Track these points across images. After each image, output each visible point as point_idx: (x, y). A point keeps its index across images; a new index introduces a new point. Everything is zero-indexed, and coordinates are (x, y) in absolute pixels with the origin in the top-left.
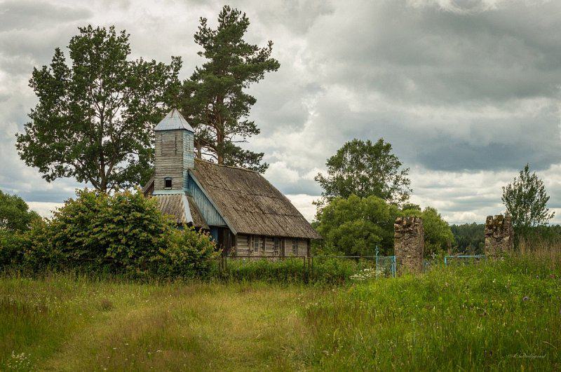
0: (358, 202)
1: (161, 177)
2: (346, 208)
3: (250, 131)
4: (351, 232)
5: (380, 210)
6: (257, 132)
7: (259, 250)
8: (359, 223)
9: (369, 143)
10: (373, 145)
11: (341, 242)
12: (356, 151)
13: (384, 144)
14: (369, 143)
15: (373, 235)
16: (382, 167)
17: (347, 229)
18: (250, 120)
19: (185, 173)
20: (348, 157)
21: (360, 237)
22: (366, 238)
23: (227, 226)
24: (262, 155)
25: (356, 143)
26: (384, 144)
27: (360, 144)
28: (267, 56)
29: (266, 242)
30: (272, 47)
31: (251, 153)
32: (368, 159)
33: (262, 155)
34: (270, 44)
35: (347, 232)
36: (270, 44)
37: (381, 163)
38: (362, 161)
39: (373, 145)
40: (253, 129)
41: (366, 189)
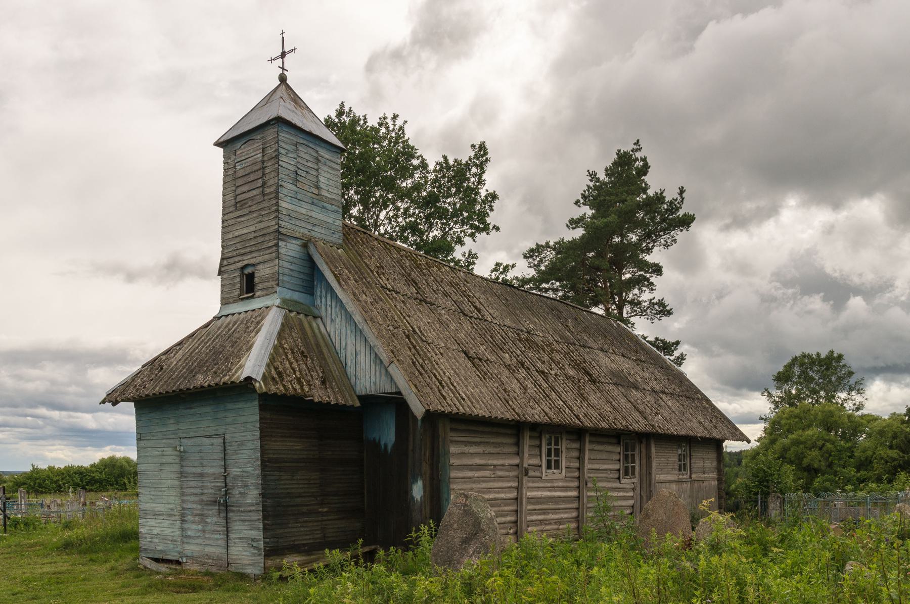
0: (809, 410)
1: (233, 267)
2: (796, 417)
3: (660, 312)
4: (802, 443)
5: (836, 418)
6: (669, 313)
7: (564, 464)
8: (815, 431)
9: (818, 354)
10: (823, 356)
11: (790, 454)
12: (805, 364)
13: (835, 355)
14: (818, 354)
15: (829, 445)
16: (834, 379)
17: (797, 440)
18: (657, 296)
19: (291, 249)
20: (797, 370)
21: (813, 447)
22: (821, 449)
23: (399, 393)
24: (677, 343)
25: (804, 356)
26: (835, 355)
27: (809, 356)
28: (677, 209)
29: (588, 446)
30: (684, 195)
31: (663, 341)
32: (818, 371)
33: (677, 343)
34: (682, 191)
35: (796, 443)
36: (682, 191)
37: (833, 374)
38: (811, 374)
39: (823, 356)
40: (662, 310)
41: (817, 401)
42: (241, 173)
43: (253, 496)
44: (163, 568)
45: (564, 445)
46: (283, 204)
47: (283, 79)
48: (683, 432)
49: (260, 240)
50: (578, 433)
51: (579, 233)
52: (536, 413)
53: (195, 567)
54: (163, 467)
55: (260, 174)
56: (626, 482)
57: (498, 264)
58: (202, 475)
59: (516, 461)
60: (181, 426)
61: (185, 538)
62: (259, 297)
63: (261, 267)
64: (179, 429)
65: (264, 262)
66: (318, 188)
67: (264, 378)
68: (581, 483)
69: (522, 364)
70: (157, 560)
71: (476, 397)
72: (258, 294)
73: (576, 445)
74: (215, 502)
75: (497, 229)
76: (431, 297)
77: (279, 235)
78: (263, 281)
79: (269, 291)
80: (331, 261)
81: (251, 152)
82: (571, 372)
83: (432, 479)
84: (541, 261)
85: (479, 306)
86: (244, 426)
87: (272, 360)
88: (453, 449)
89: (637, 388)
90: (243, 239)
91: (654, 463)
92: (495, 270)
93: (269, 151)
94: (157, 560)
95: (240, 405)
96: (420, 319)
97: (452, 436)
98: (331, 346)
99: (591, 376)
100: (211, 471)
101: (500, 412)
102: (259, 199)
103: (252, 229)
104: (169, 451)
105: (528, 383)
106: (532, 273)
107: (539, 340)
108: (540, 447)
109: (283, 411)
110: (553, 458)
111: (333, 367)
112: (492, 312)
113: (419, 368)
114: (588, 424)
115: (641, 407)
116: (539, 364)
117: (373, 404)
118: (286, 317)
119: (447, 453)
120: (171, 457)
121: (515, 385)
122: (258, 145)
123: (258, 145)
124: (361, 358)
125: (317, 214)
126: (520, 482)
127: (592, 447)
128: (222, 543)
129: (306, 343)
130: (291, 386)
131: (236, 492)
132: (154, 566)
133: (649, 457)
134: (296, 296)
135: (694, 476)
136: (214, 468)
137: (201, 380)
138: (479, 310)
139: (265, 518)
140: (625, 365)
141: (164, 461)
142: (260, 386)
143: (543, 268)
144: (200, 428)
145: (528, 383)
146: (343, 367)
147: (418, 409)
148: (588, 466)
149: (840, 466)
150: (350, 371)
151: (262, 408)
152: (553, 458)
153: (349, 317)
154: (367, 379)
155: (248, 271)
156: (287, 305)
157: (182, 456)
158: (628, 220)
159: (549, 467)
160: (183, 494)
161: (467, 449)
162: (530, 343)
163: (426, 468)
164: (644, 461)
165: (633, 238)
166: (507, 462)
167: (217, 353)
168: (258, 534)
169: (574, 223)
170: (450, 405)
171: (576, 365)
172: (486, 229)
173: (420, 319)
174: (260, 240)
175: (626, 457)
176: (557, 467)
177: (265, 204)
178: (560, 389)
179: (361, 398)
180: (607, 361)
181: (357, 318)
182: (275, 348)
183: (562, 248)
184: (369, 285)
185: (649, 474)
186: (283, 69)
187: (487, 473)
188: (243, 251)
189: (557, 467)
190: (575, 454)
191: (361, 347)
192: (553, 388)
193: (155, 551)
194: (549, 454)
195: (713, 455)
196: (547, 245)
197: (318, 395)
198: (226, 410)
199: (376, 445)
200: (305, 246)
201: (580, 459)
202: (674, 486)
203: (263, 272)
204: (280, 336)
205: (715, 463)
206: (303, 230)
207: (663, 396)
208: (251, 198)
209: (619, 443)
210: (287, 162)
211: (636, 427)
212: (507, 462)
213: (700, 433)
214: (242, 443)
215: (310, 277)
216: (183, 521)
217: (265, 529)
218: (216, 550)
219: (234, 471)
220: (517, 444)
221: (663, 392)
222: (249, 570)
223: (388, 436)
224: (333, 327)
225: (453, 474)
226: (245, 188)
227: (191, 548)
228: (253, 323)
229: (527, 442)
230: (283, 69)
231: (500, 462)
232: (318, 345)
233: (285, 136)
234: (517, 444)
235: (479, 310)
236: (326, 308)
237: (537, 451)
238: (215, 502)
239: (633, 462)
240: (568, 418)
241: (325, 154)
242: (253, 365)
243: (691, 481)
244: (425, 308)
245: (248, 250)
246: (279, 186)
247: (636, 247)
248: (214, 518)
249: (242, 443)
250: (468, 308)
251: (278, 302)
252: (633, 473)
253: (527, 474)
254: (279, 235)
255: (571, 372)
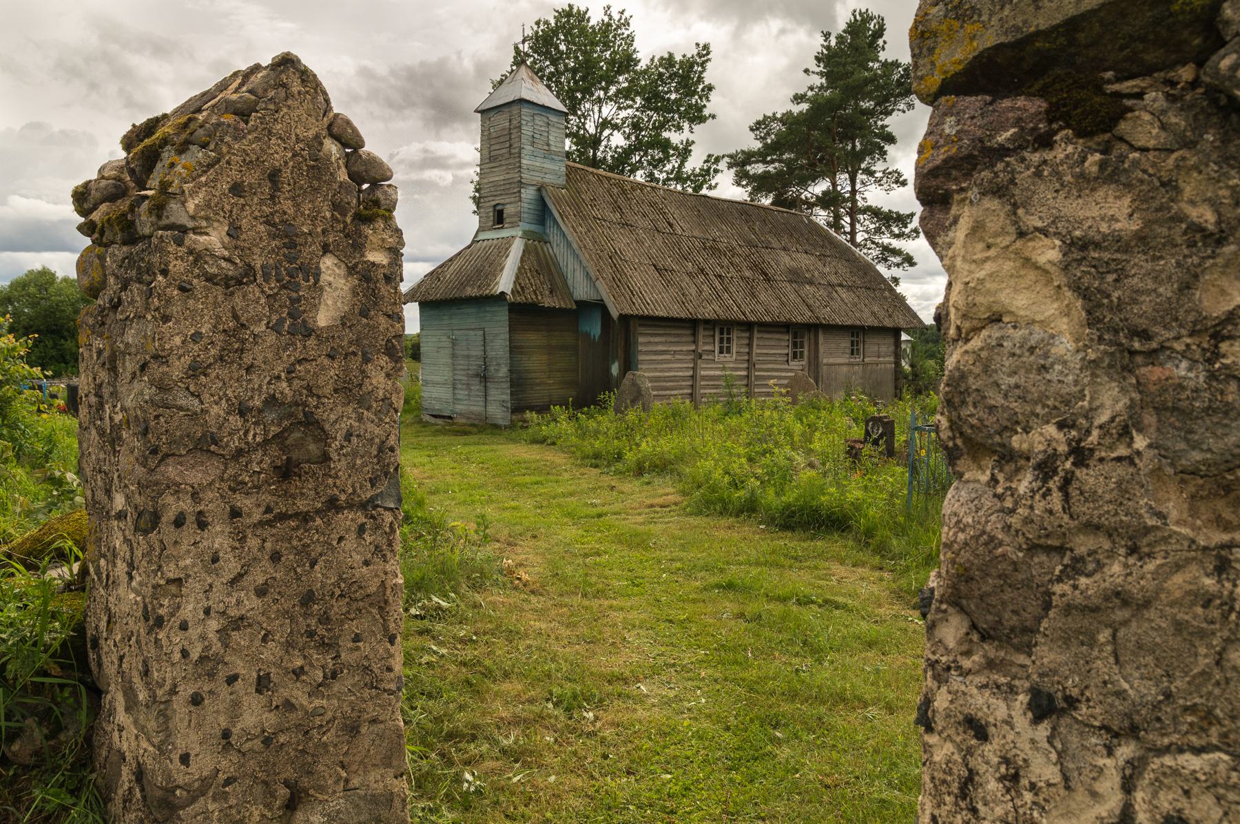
7: (734, 350)
19: (528, 194)
29: (756, 335)
42: (494, 135)
43: (504, 371)
44: (440, 421)
45: (735, 335)
46: (524, 161)
48: (849, 323)
50: (748, 326)
51: (805, 107)
52: (708, 311)
53: (464, 421)
55: (507, 138)
56: (795, 365)
57: (709, 156)
58: (468, 356)
59: (693, 348)
61: (456, 400)
66: (548, 145)
67: (513, 292)
68: (751, 365)
69: (702, 270)
70: (435, 416)
71: (660, 302)
73: (747, 335)
74: (477, 375)
75: (714, 117)
76: (632, 219)
77: (521, 184)
78: (511, 216)
79: (514, 225)
80: (558, 201)
81: (501, 121)
82: (747, 274)
83: (625, 361)
84: (768, 134)
85: (671, 220)
86: (498, 323)
87: (517, 278)
88: (641, 340)
89: (811, 283)
90: (495, 184)
91: (822, 349)
92: (706, 162)
93: (515, 122)
94: (435, 416)
96: (622, 241)
97: (641, 330)
98: (557, 265)
99: (766, 275)
100: (474, 353)
101: (676, 311)
102: (507, 155)
104: (444, 338)
105: (705, 288)
106: (757, 145)
107: (722, 246)
108: (714, 336)
109: (524, 313)
110: (725, 345)
111: (558, 281)
112: (684, 226)
113: (618, 281)
114: (752, 318)
115: (811, 302)
116: (718, 270)
117: (585, 307)
118: (526, 245)
119: (636, 343)
120: (446, 343)
121: (693, 290)
122: (506, 116)
123: (506, 116)
124: (577, 273)
125: (548, 165)
126: (696, 364)
127: (760, 335)
128: (482, 403)
129: (540, 264)
130: (530, 297)
131: (492, 368)
132: (433, 420)
133: (817, 344)
134: (533, 227)
135: (867, 360)
136: (477, 352)
137: (470, 291)
138: (671, 225)
139: (511, 386)
140: (804, 261)
142: (510, 297)
143: (769, 141)
144: (467, 324)
145: (705, 288)
146: (565, 281)
147: (615, 313)
148: (756, 350)
150: (570, 282)
151: (510, 311)
152: (725, 345)
153: (569, 245)
154: (582, 291)
155: (499, 208)
156: (527, 235)
157: (454, 343)
158: (857, 91)
159: (721, 352)
160: (454, 369)
161: (652, 339)
162: (715, 251)
163: (621, 353)
164: (813, 346)
165: (867, 104)
166: (685, 348)
167: (479, 271)
168: (507, 397)
169: (798, 98)
170: (639, 309)
171: (755, 267)
172: (702, 119)
173: (622, 241)
175: (795, 345)
176: (728, 351)
177: (511, 161)
178: (733, 289)
179: (576, 302)
180: (787, 259)
181: (575, 246)
182: (519, 269)
183: (787, 119)
184: (584, 218)
185: (817, 357)
187: (668, 357)
189: (728, 351)
190: (746, 341)
191: (577, 266)
192: (726, 290)
193: (434, 410)
194: (721, 341)
195: (891, 341)
196: (774, 118)
197: (548, 302)
199: (587, 335)
200: (539, 190)
201: (750, 345)
202: (845, 369)
203: (509, 210)
204: (522, 260)
205: (892, 348)
206: (537, 178)
207: (839, 289)
208: (502, 155)
209: (788, 332)
210: (527, 130)
211: (799, 319)
212: (685, 348)
213: (870, 321)
214: (496, 335)
215: (542, 212)
216: (454, 388)
217: (512, 394)
218: (477, 408)
219: (491, 354)
220: (694, 335)
221: (841, 285)
222: (501, 422)
223: (595, 330)
224: (558, 250)
225: (641, 358)
226: (497, 147)
227: (460, 408)
228: (503, 248)
229: (702, 333)
231: (679, 348)
232: (547, 264)
233: (525, 111)
234: (694, 335)
235: (671, 225)
236: (554, 236)
237: (711, 340)
238: (477, 375)
239: (802, 347)
240: (736, 314)
241: (553, 118)
242: (505, 283)
243: (865, 365)
244: (626, 231)
246: (521, 148)
247: (870, 113)
248: (476, 387)
249: (496, 335)
250: (662, 225)
251: (520, 233)
252: (802, 356)
253: (700, 357)
254: (521, 184)
255: (747, 274)
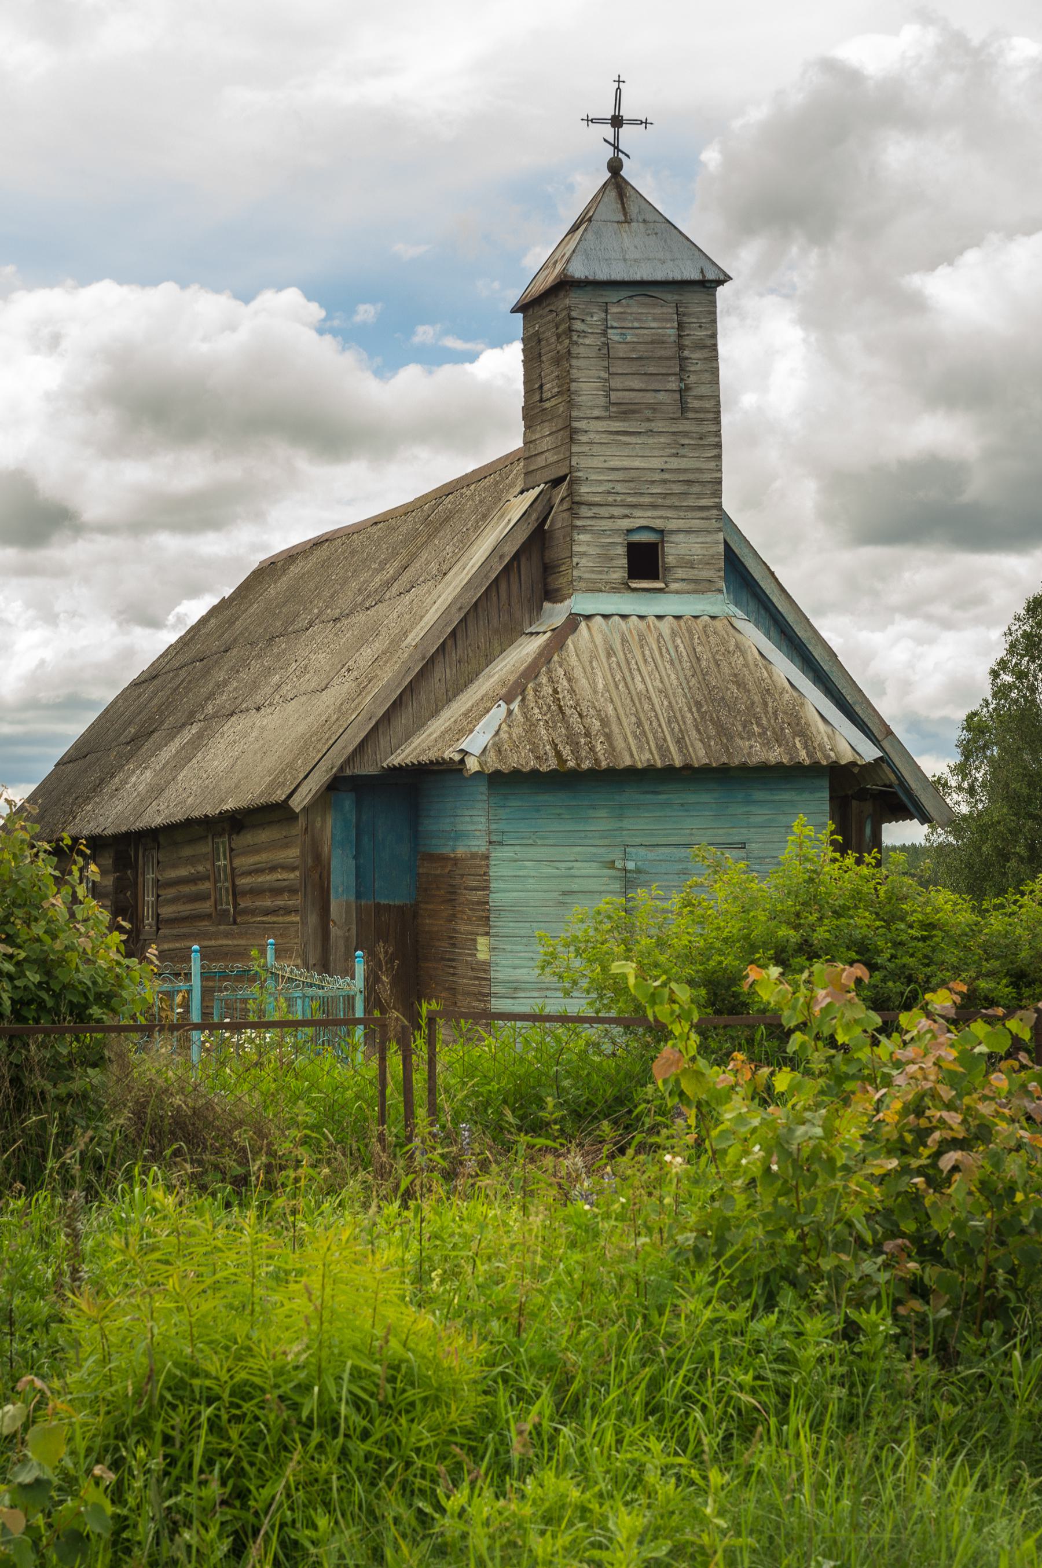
47: (615, 167)
49: (677, 488)
54: (568, 899)
60: (626, 824)
62: (677, 592)
63: (680, 538)
64: (621, 829)
65: (688, 532)
72: (674, 586)
95: (786, 796)
103: (657, 463)
141: (575, 887)
149: (371, 1375)
174: (677, 488)
186: (616, 147)
188: (630, 499)
198: (749, 802)
230: (616, 147)
245: (647, 500)
